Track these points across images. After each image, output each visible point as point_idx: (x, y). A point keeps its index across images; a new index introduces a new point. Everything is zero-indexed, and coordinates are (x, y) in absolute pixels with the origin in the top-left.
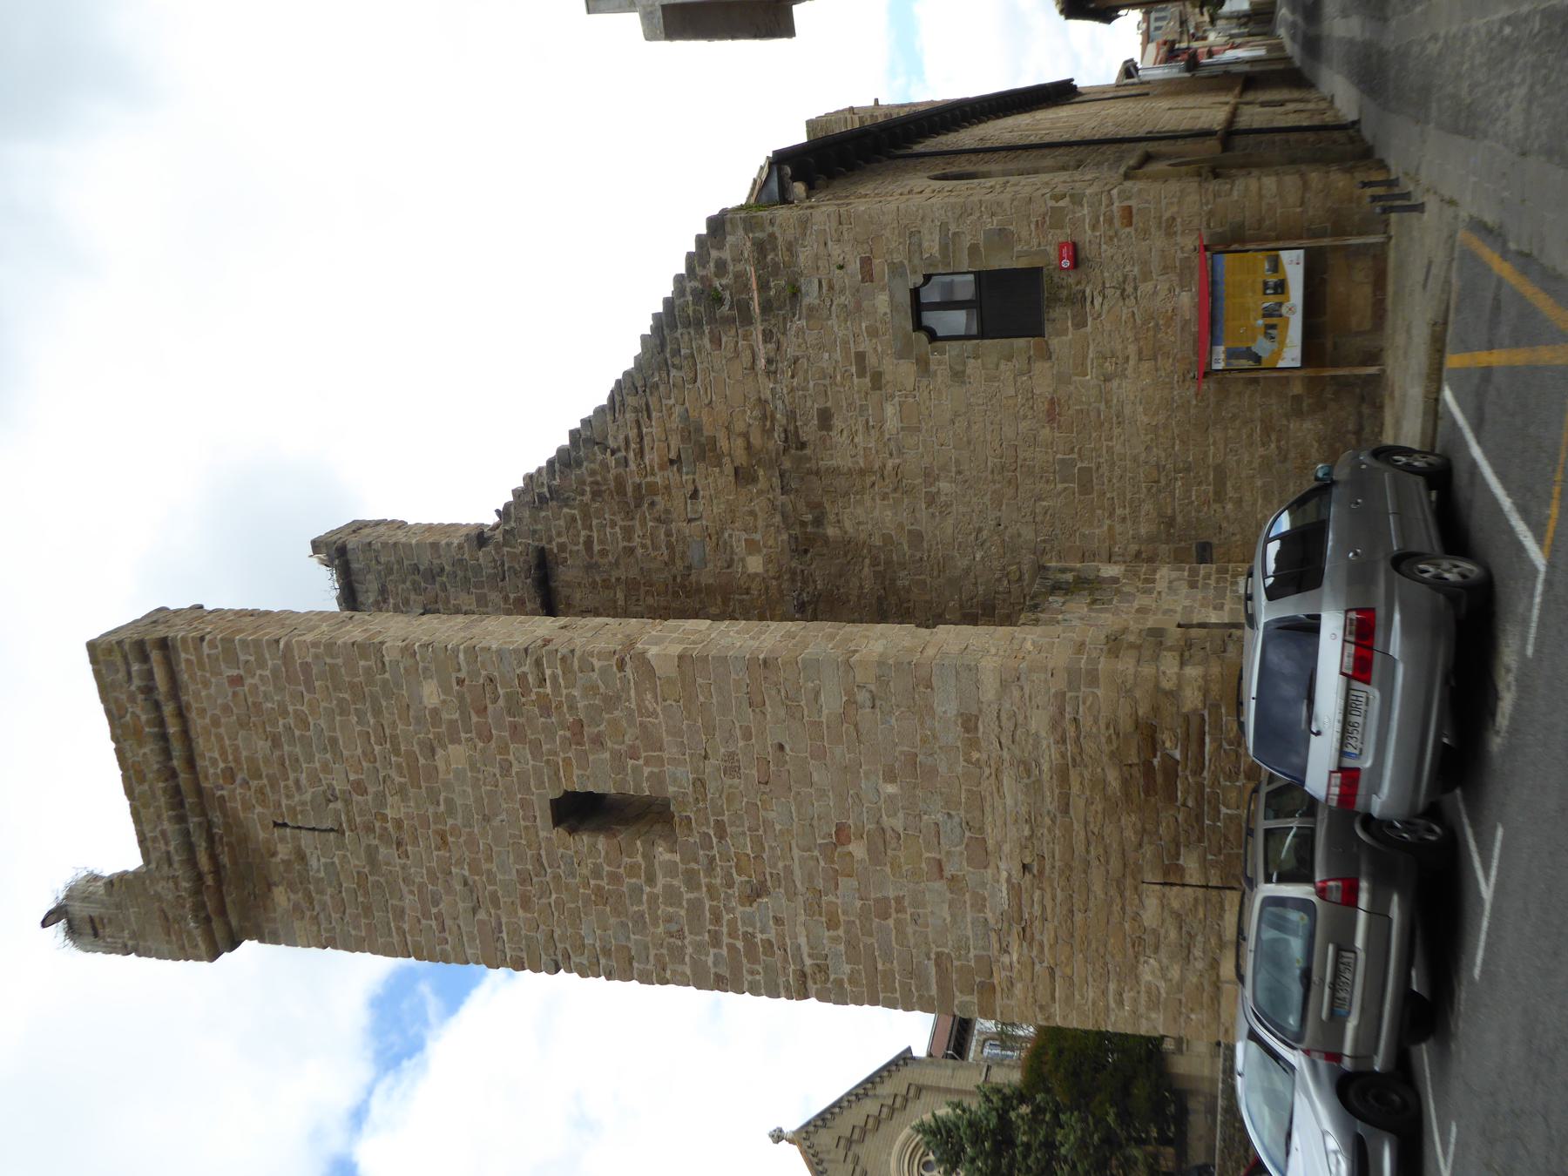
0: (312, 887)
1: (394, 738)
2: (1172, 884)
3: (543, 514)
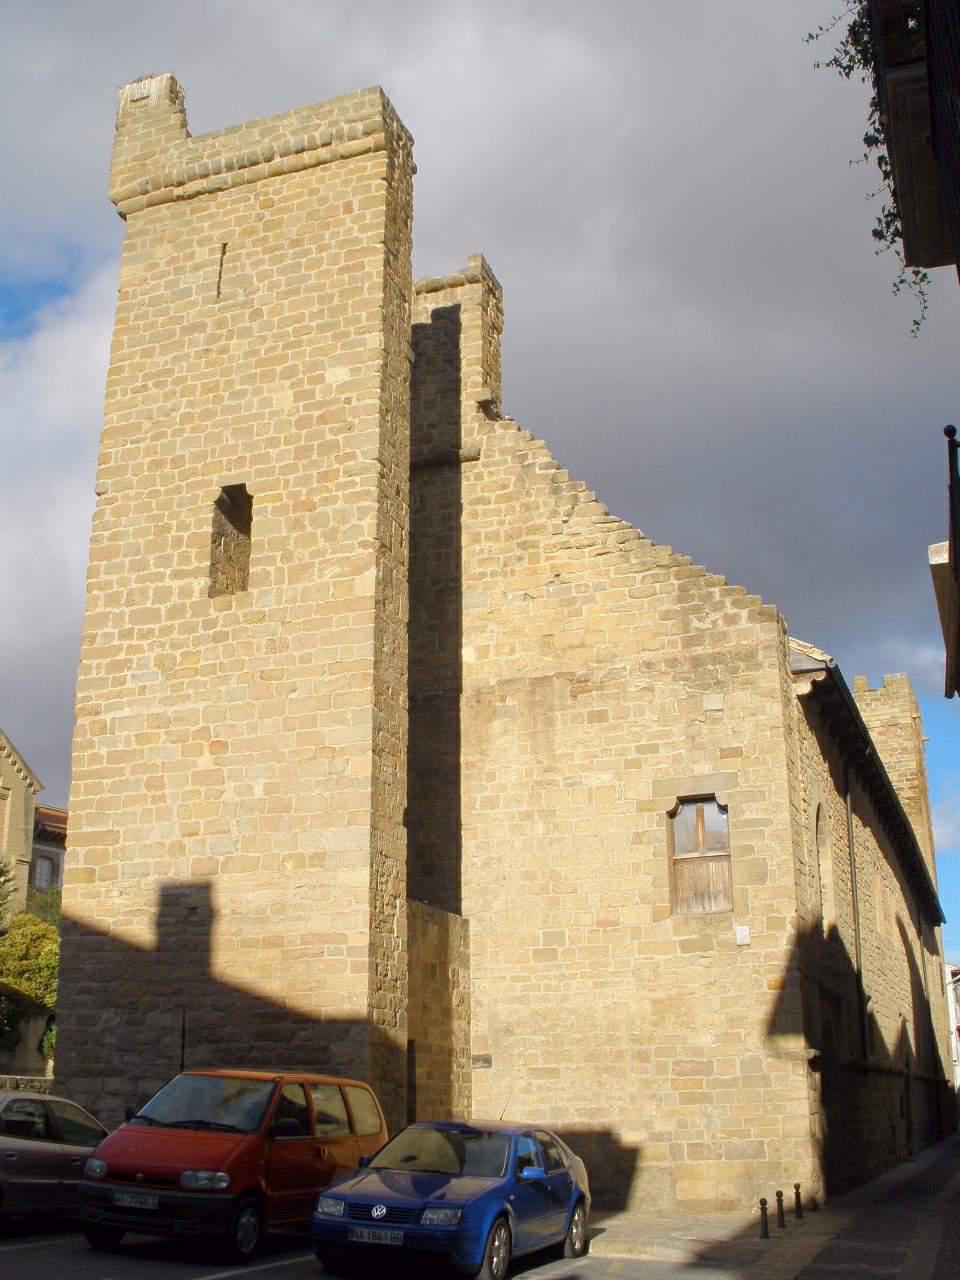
0: (171, 277)
1: (299, 344)
2: (183, 1037)
3: (509, 458)
